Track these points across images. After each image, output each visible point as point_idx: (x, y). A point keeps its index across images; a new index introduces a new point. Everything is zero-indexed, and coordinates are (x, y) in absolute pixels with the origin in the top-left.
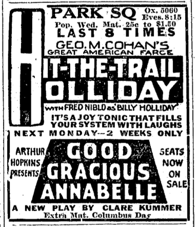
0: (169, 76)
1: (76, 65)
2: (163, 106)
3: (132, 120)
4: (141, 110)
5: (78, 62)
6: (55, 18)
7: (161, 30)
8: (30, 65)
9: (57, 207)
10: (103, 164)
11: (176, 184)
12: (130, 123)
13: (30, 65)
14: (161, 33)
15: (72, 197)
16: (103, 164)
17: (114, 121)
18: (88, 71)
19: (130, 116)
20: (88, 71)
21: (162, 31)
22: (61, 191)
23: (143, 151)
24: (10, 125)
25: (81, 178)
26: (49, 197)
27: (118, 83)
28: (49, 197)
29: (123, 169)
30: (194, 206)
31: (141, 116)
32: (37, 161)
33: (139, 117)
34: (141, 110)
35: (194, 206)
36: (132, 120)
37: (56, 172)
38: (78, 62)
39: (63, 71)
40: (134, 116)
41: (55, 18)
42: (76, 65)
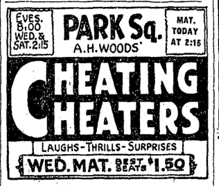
0: (80, 93)
1: (132, 112)
2: (65, 151)
4: (93, 45)
5: (134, 109)
7: (49, 163)
8: (65, 39)
10: (61, 94)
11: (52, 148)
13: (65, 39)
15: (70, 66)
16: (61, 94)
22: (164, 78)
26: (109, 131)
27: (153, 66)
28: (109, 131)
29: (7, 115)
30: (8, 152)
32: (75, 146)
34: (93, 45)
35: (8, 152)
37: (193, 79)
38: (134, 109)
42: (132, 112)
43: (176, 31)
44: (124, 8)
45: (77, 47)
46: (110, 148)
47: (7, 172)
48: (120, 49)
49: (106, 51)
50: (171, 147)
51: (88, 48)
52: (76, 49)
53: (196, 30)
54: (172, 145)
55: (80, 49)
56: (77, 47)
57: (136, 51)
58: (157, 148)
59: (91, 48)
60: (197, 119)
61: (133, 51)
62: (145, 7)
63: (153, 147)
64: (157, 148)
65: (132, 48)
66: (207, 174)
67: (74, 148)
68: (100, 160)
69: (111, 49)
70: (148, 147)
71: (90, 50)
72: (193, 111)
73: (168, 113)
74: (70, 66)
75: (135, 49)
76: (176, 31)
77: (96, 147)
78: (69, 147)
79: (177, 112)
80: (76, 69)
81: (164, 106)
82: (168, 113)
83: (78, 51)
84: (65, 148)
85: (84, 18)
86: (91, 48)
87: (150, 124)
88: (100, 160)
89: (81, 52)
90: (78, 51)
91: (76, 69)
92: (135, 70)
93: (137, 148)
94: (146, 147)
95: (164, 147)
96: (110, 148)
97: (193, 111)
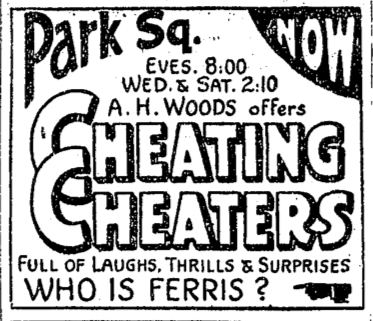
34: (148, 101)
44: (11, 146)
45: (115, 105)
46: (213, 266)
47: (10, 36)
48: (205, 108)
49: (179, 113)
50: (339, 267)
51: (139, 106)
52: (111, 108)
54: (343, 264)
55: (119, 108)
56: (115, 105)
57: (302, 114)
58: (312, 267)
59: (142, 106)
60: (309, 209)
61: (228, 114)
63: (305, 266)
64: (312, 267)
66: (180, 199)
67: (148, 266)
69: (201, 110)
70: (295, 266)
71: (143, 110)
73: (293, 211)
75: (230, 111)
77: (185, 265)
78: (140, 265)
82: (293, 211)
83: (115, 112)
84: (133, 265)
85: (65, 26)
86: (142, 106)
87: (261, 229)
89: (120, 114)
90: (115, 112)
94: (291, 267)
95: (326, 267)
96: (213, 266)
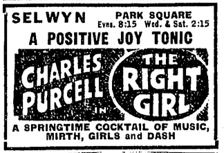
1: (151, 59)
3: (67, 130)
6: (185, 105)
7: (27, 16)
8: (177, 82)
9: (35, 126)
12: (67, 134)
13: (177, 82)
14: (27, 20)
17: (52, 131)
18: (42, 80)
19: (41, 22)
20: (42, 80)
21: (28, 18)
23: (70, 112)
24: (206, 50)
25: (55, 79)
31: (75, 138)
33: (77, 138)
36: (67, 130)
39: (87, 73)
40: (86, 34)
41: (185, 105)
43: (160, 37)
53: (138, 36)
62: (6, 91)
65: (65, 39)
68: (65, 125)
72: (98, 60)
74: (164, 55)
75: (99, 127)
76: (160, 37)
79: (179, 101)
80: (167, 57)
81: (165, 96)
82: (169, 101)
88: (65, 125)
91: (167, 57)
92: (32, 66)
93: (186, 127)
97: (98, 60)
